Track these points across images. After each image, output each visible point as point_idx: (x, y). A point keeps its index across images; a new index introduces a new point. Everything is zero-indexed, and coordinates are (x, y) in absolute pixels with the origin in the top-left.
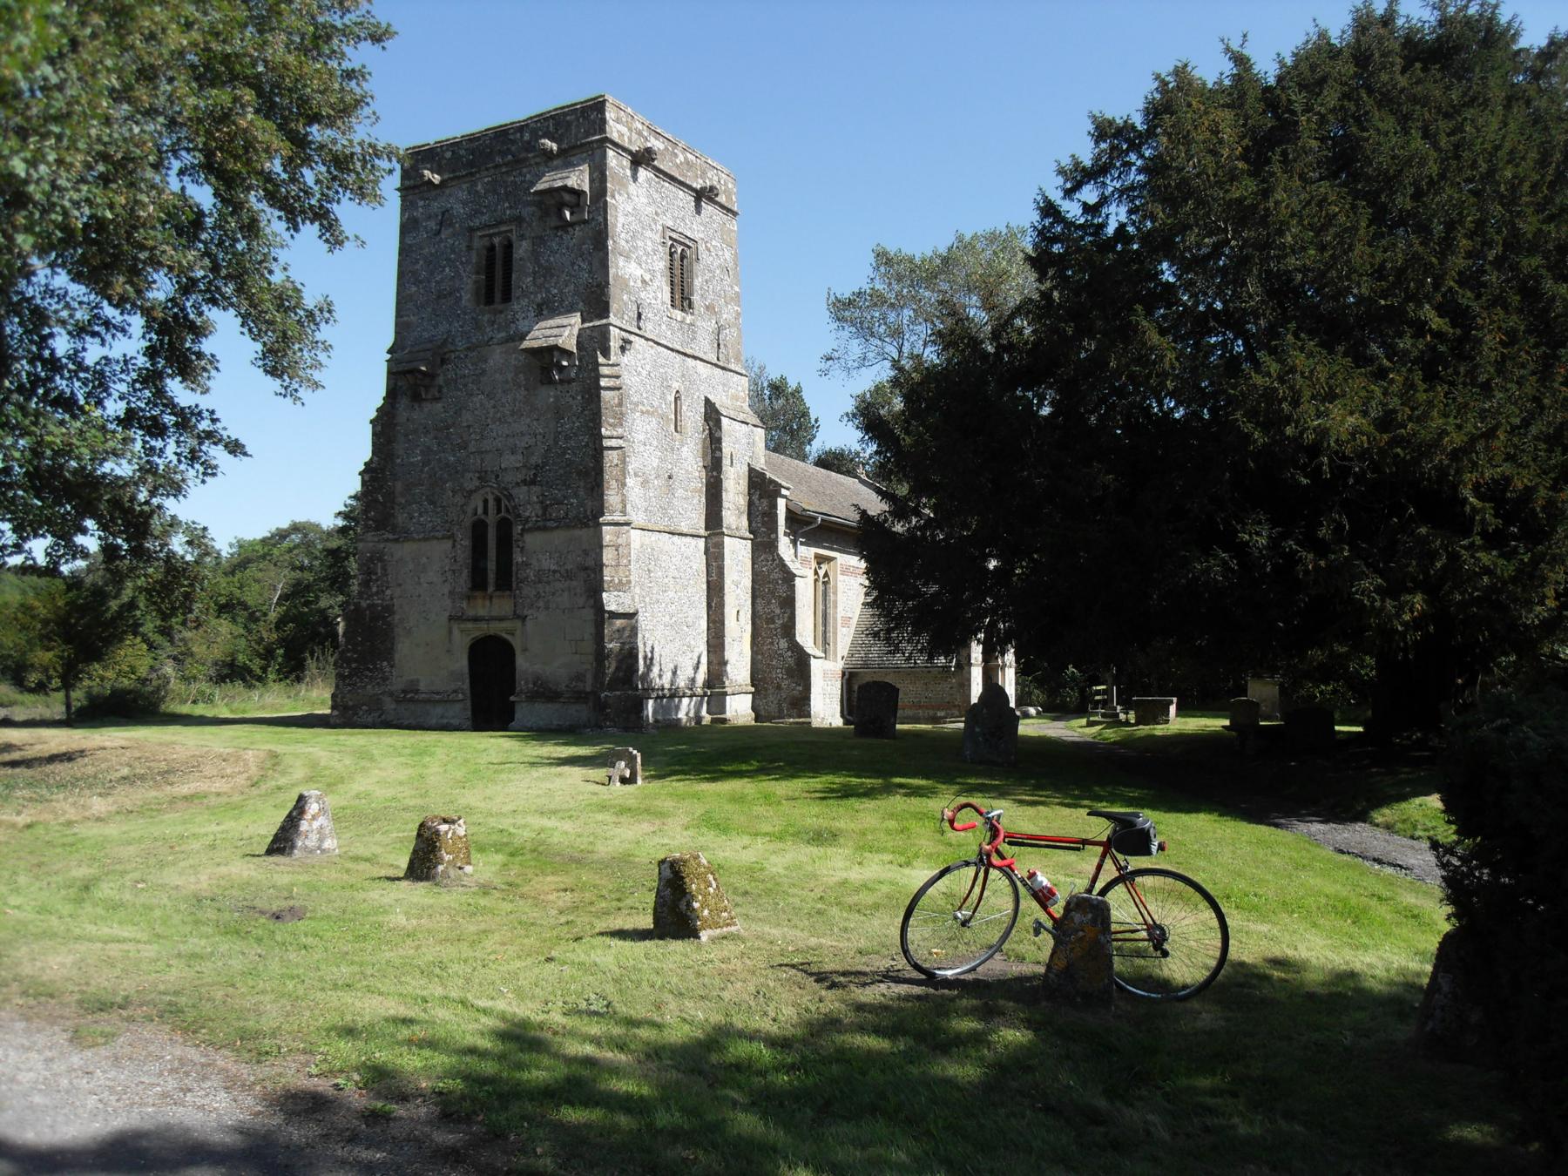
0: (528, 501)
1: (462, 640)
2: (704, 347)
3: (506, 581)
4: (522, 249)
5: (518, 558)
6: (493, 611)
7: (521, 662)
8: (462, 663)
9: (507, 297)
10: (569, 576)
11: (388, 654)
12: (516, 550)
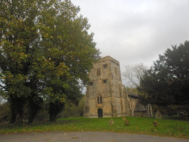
0: (103, 95)
1: (97, 109)
2: (118, 79)
3: (101, 102)
4: (101, 70)
5: (103, 100)
6: (100, 105)
7: (103, 111)
8: (97, 111)
9: (100, 75)
10: (108, 102)
11: (89, 111)
12: (102, 100)
